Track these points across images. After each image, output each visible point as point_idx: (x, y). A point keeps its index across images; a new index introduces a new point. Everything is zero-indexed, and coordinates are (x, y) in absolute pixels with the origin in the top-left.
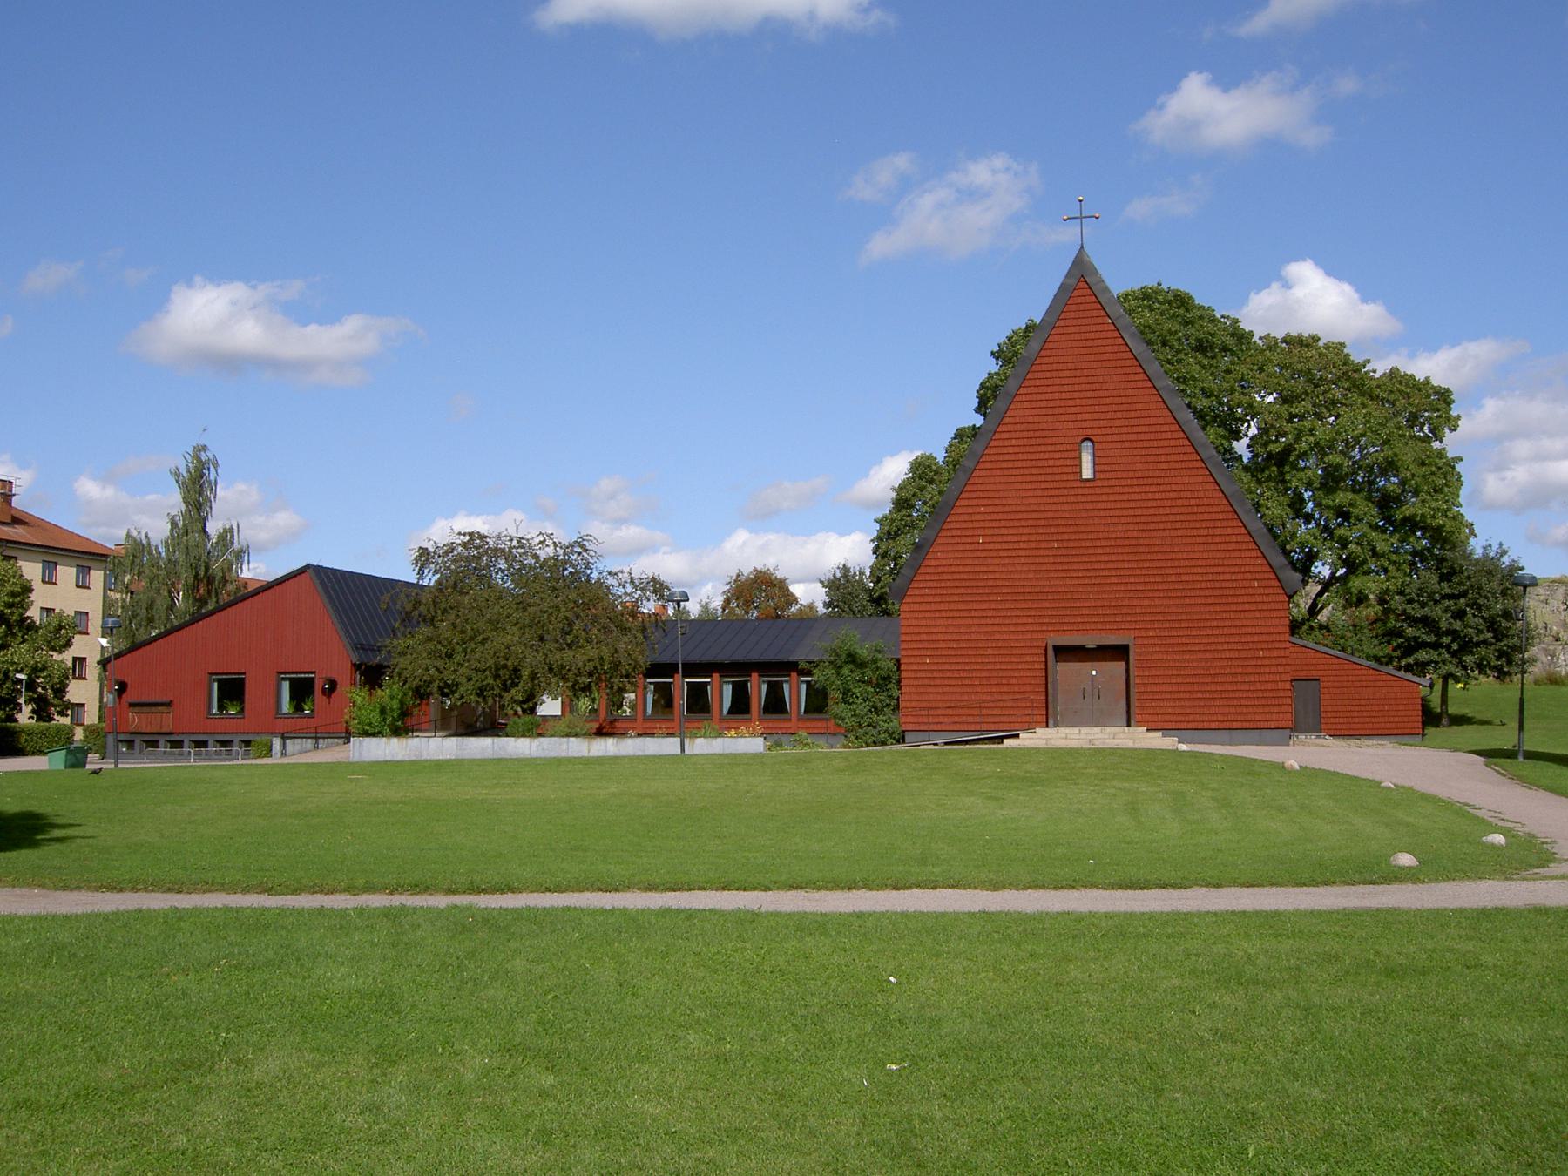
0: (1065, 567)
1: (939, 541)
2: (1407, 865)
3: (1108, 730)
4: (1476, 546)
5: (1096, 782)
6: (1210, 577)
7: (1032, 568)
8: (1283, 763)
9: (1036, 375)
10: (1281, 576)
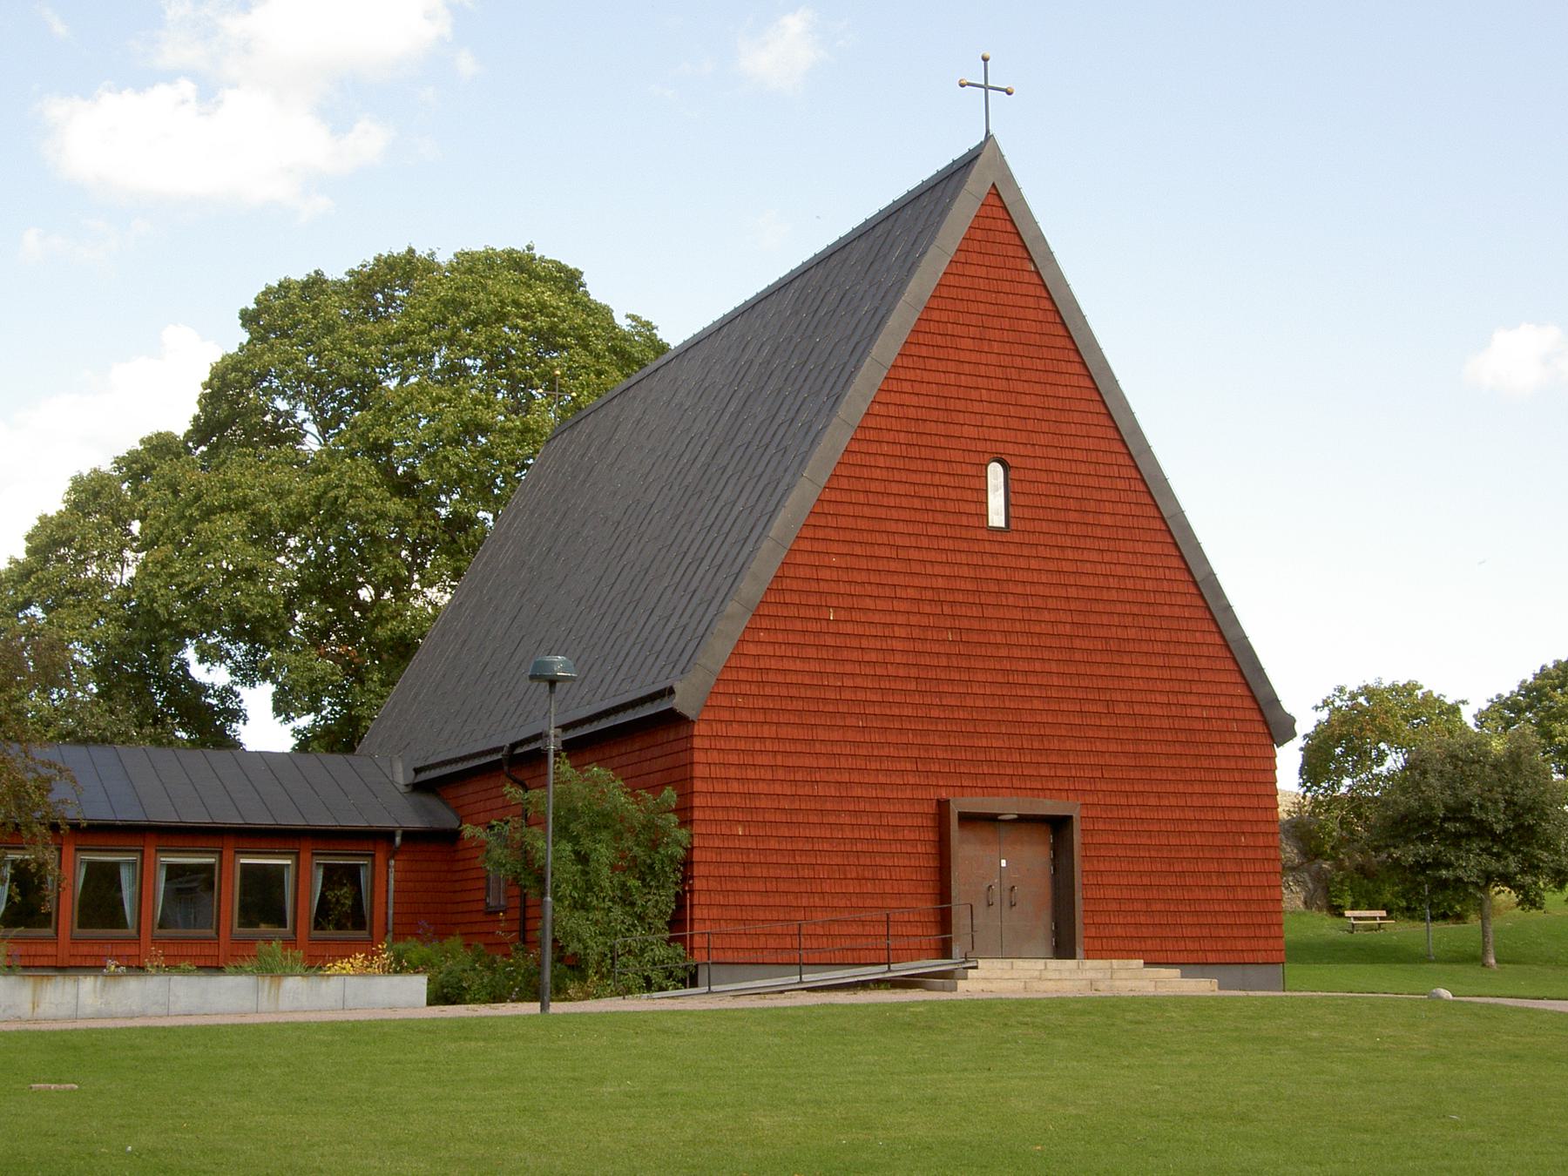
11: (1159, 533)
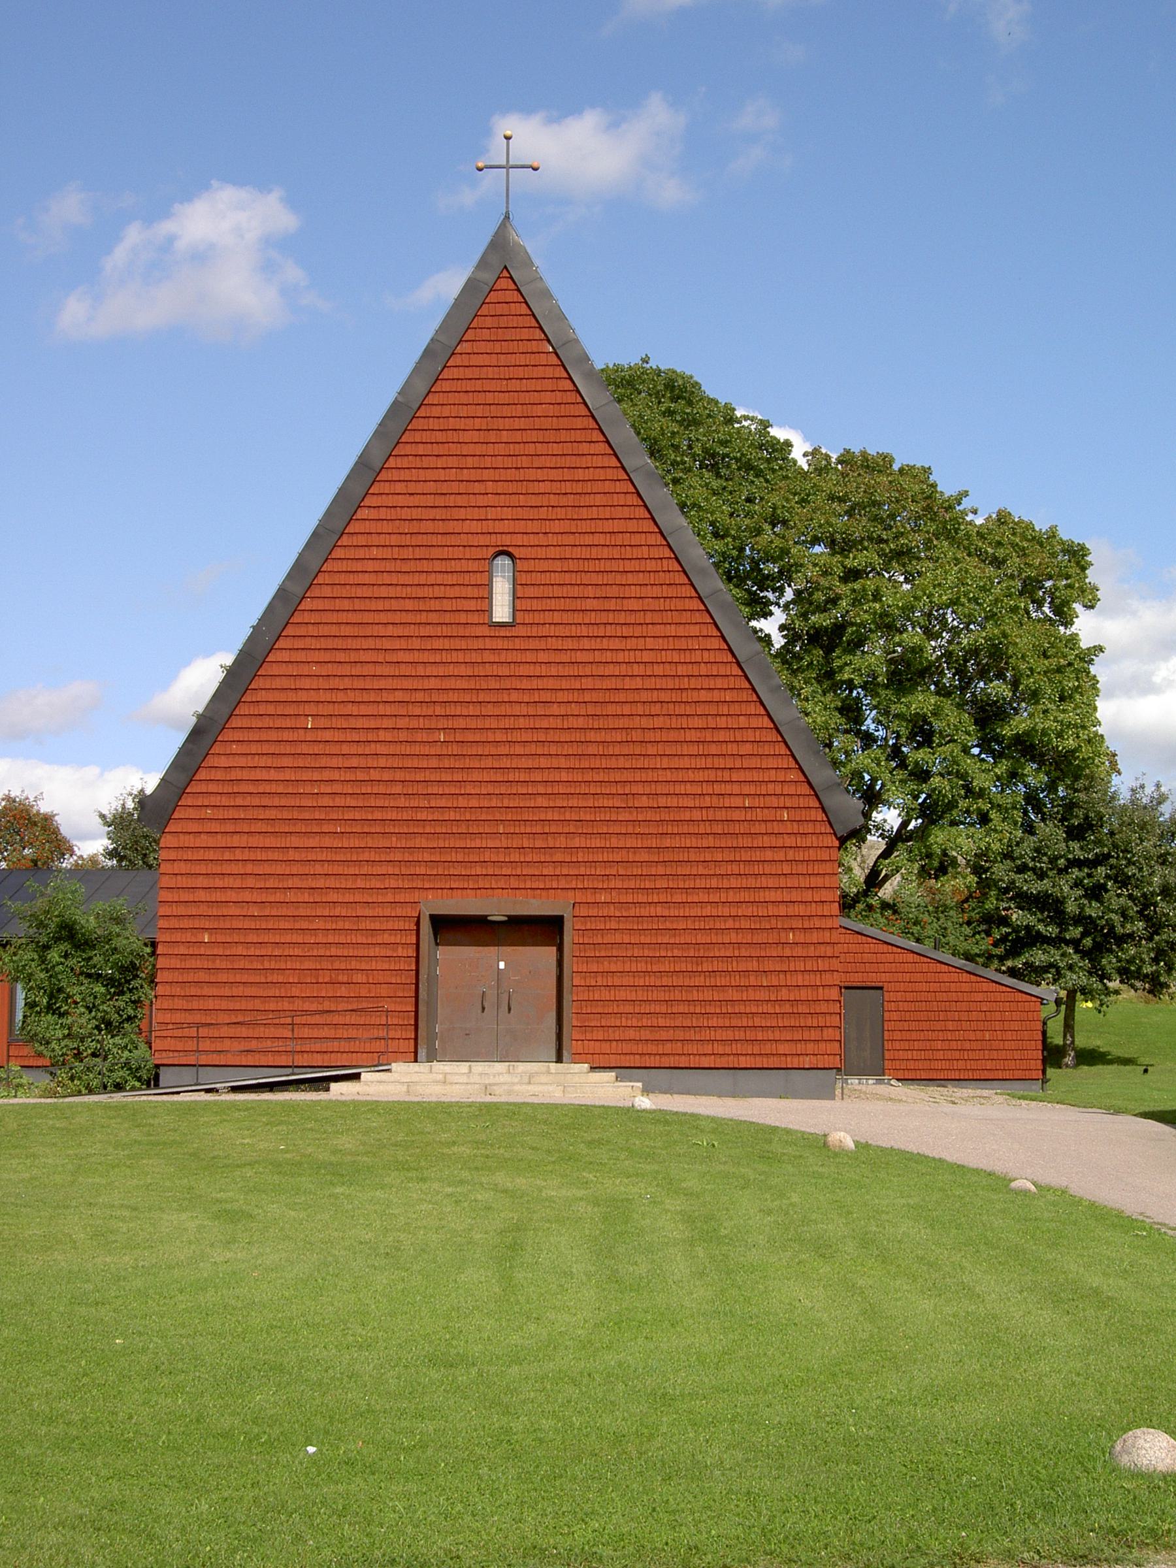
0: (458, 777)
1: (235, 723)
2: (1161, 1467)
3: (521, 1067)
4: (1122, 785)
5: (465, 1174)
6: (707, 801)
7: (399, 775)
8: (825, 1135)
9: (418, 437)
10: (826, 803)
11: (697, 614)
